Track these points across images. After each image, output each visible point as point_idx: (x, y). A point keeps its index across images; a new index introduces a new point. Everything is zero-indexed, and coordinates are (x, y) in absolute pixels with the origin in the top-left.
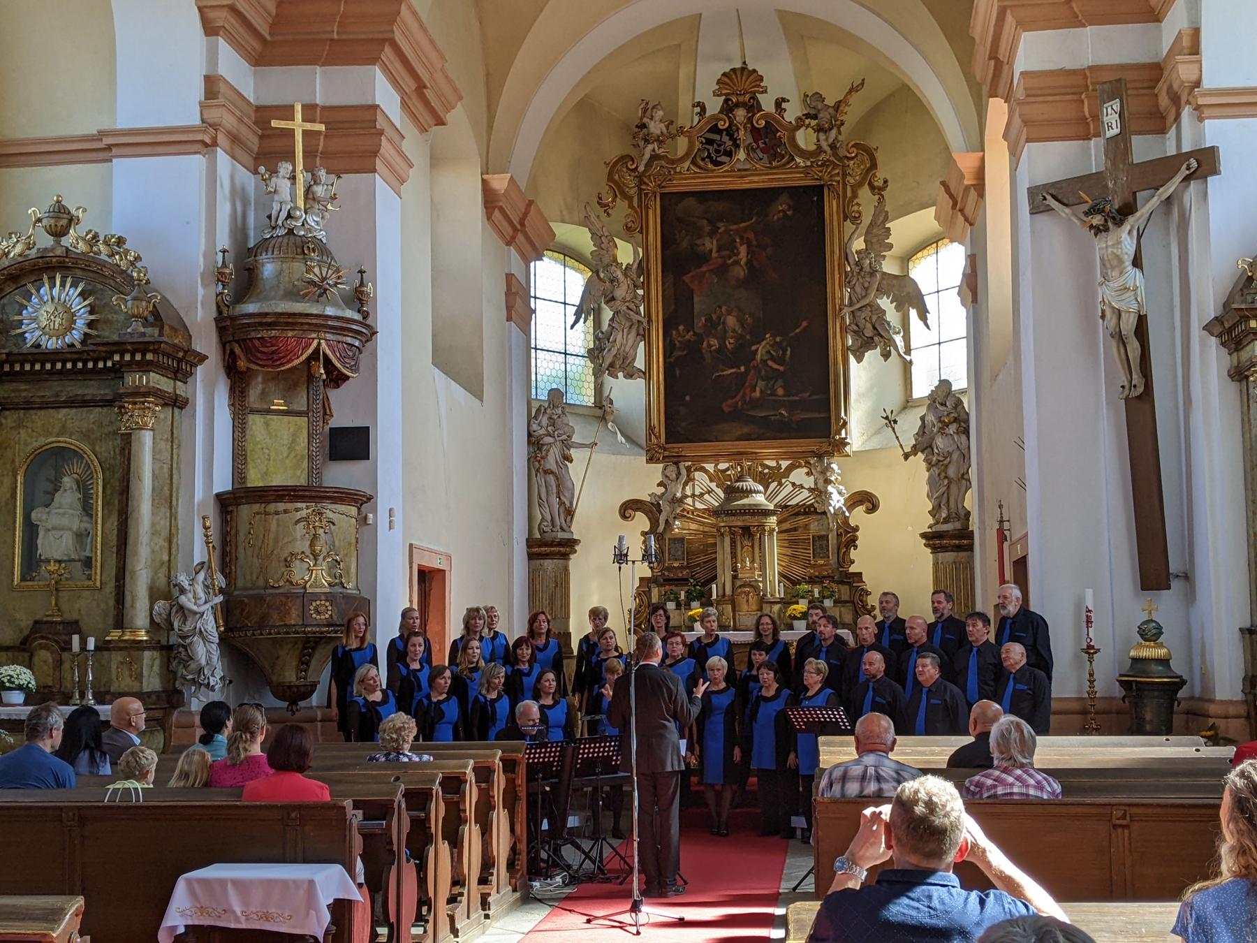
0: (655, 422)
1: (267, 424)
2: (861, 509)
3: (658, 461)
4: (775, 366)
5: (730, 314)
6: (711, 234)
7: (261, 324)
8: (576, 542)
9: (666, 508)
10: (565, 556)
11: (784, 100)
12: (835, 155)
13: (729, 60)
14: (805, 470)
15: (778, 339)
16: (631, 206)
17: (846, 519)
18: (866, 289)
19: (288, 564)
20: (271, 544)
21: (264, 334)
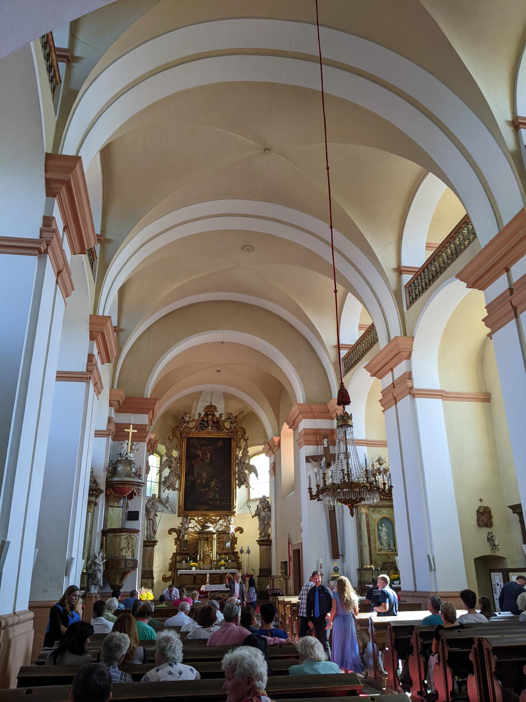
0: (181, 504)
1: (113, 510)
2: (238, 532)
3: (181, 516)
4: (216, 489)
5: (204, 473)
6: (200, 450)
7: (120, 484)
8: (157, 541)
9: (183, 531)
10: (153, 546)
11: (222, 414)
12: (235, 430)
13: (207, 402)
14: (224, 520)
15: (218, 481)
16: (178, 440)
17: (234, 535)
18: (242, 468)
19: (122, 550)
20: (117, 544)
21: (120, 486)
